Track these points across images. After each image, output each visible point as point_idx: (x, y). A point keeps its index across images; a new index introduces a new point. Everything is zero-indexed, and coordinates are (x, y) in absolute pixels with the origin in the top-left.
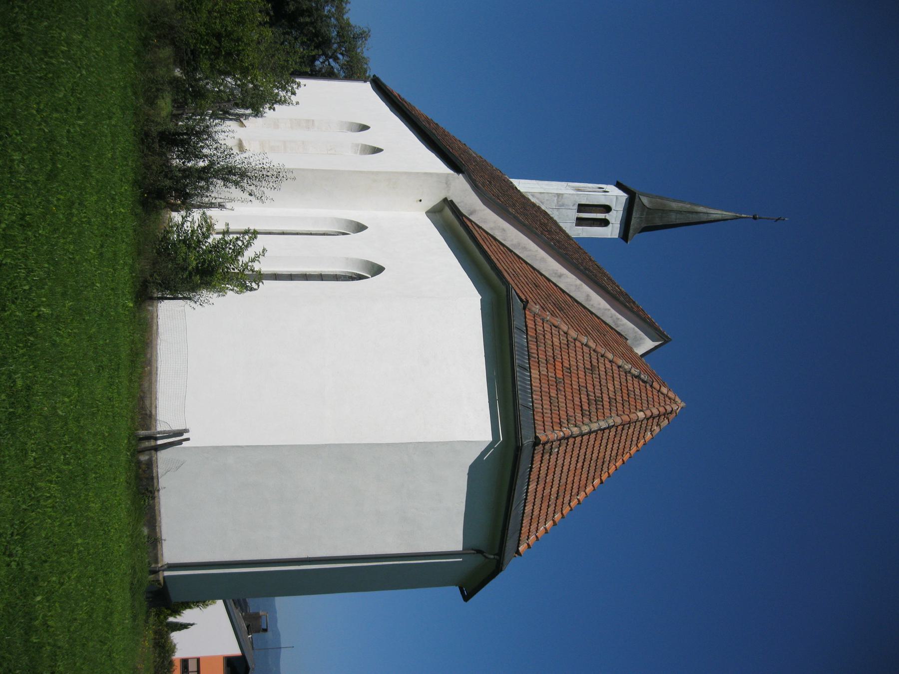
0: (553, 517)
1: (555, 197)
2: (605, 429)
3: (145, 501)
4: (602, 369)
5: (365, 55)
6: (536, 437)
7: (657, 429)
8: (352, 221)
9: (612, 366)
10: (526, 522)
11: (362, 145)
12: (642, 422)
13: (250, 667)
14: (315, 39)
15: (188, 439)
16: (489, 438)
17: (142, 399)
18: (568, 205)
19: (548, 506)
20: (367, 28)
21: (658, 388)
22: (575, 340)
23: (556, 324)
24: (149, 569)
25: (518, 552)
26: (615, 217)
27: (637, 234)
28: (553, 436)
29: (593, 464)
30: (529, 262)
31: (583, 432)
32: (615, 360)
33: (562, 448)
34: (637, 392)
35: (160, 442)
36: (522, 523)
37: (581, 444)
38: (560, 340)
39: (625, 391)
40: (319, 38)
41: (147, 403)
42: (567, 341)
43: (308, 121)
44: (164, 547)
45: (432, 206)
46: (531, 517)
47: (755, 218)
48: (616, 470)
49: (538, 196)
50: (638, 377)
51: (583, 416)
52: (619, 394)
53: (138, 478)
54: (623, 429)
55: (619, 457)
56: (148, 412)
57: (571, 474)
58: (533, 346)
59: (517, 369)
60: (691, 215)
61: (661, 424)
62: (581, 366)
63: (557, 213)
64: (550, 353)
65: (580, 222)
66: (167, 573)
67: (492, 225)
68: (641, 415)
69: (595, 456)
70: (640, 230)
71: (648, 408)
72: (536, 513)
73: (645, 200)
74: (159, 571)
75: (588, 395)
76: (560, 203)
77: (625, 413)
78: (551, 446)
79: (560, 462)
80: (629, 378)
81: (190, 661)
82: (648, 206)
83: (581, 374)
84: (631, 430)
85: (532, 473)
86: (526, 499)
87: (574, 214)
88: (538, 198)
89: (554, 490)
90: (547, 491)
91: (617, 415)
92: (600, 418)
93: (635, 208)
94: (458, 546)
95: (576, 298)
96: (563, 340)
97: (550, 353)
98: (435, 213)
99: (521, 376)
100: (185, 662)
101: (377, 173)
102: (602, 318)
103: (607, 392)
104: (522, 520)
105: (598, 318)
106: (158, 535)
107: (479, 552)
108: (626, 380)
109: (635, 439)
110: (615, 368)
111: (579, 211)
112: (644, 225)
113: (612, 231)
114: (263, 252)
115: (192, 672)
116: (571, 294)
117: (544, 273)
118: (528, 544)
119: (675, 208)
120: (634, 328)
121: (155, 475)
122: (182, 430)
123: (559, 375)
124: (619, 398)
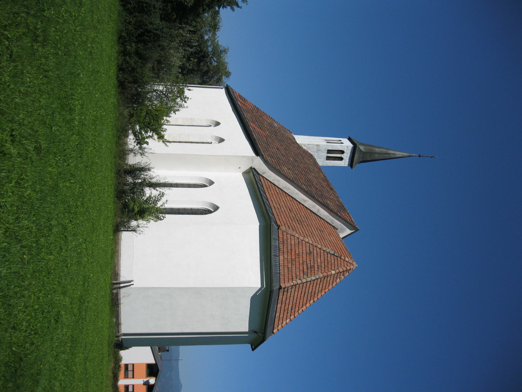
0: (290, 317)
1: (316, 146)
2: (314, 280)
3: (115, 308)
4: (315, 252)
5: (226, 61)
6: (280, 286)
7: (342, 277)
8: (208, 179)
9: (320, 251)
10: (276, 320)
11: (215, 136)
12: (334, 275)
13: (159, 369)
14: (200, 53)
15: (133, 284)
16: (260, 286)
17: (115, 267)
18: (322, 150)
19: (287, 313)
20: (227, 46)
21: (344, 259)
22: (302, 241)
23: (293, 234)
24: (115, 335)
25: (273, 333)
26: (346, 157)
27: (358, 164)
28: (287, 285)
29: (309, 294)
30: (291, 195)
31: (303, 282)
32: (322, 248)
33: (293, 290)
34: (333, 261)
35: (121, 285)
36: (275, 321)
37: (303, 287)
38: (295, 241)
39: (326, 262)
40: (202, 53)
41: (117, 268)
42: (298, 242)
43: (191, 119)
44: (122, 326)
45: (245, 170)
46: (279, 318)
47: (419, 156)
48: (322, 296)
49: (307, 145)
50: (334, 255)
51: (304, 275)
52: (323, 263)
53: (112, 300)
54: (324, 279)
55: (323, 290)
56: (117, 272)
57: (298, 300)
58: (281, 246)
59: (272, 257)
60: (386, 155)
61: (345, 275)
62: (304, 252)
63: (317, 154)
64: (289, 248)
65: (328, 158)
66: (123, 337)
67: (273, 178)
68: (333, 272)
69: (310, 291)
70: (359, 163)
71: (338, 268)
72: (281, 316)
73: (362, 148)
74: (119, 336)
75: (307, 265)
76: (318, 149)
77: (326, 272)
78: (288, 289)
79: (292, 295)
80: (329, 255)
81: (129, 365)
82: (363, 151)
83: (304, 256)
84: (328, 279)
85: (279, 300)
86: (276, 311)
87: (325, 155)
88: (307, 147)
89: (290, 306)
90: (286, 307)
91: (321, 273)
92: (312, 275)
93: (356, 152)
94: (247, 330)
95: (313, 211)
96: (296, 241)
97: (289, 248)
98: (246, 174)
99: (275, 259)
100: (126, 366)
101: (220, 156)
102: (325, 219)
103: (317, 263)
104: (275, 319)
105: (324, 220)
106: (120, 322)
107: (255, 332)
108: (327, 256)
109: (331, 282)
110: (322, 251)
111: (328, 153)
112: (361, 160)
113: (345, 163)
114: (166, 202)
115: (130, 371)
116: (311, 209)
117: (297, 200)
118: (278, 329)
119: (378, 151)
120: (341, 225)
121: (119, 298)
122: (131, 281)
123: (293, 257)
124: (323, 265)
